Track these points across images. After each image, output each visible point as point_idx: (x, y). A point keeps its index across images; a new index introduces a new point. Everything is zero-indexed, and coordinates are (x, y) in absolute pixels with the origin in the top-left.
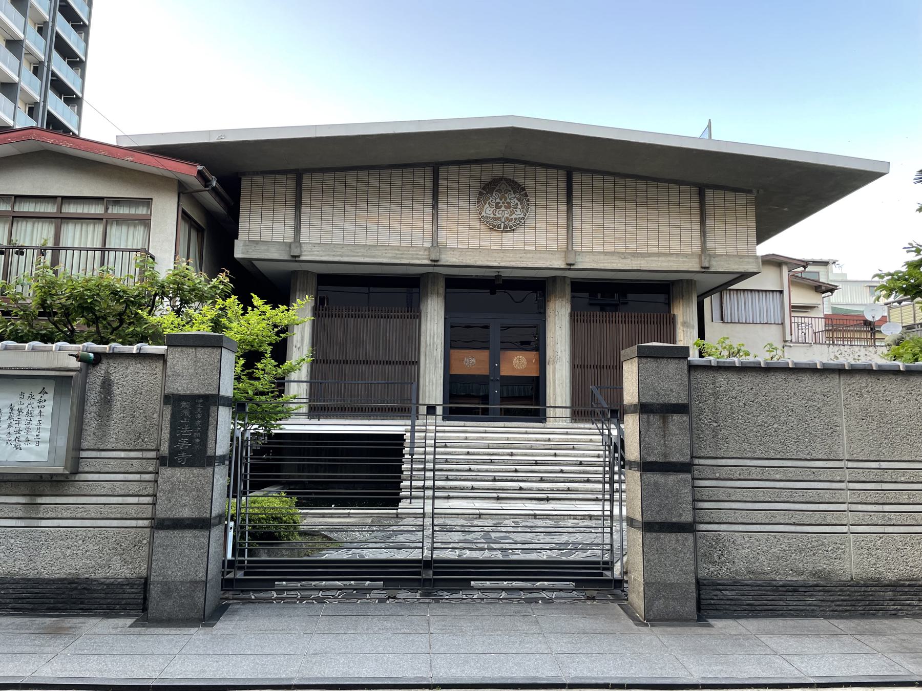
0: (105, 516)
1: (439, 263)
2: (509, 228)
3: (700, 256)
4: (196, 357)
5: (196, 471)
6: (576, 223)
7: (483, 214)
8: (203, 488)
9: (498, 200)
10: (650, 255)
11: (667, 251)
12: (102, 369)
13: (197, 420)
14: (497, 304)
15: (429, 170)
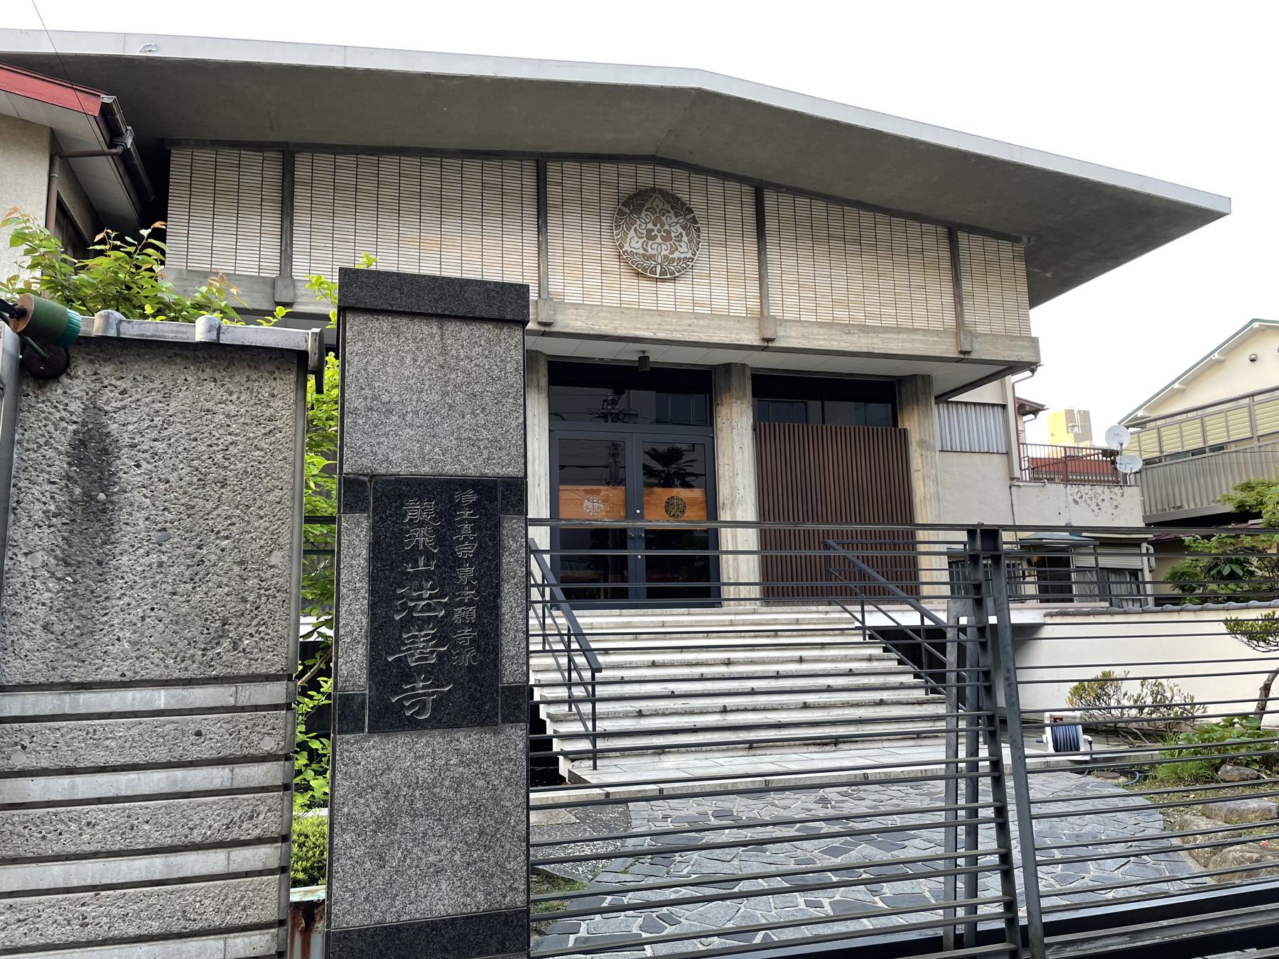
0: (102, 933)
1: (553, 329)
2: (668, 275)
3: (957, 335)
4: (444, 351)
5: (467, 740)
6: (773, 271)
7: (627, 247)
8: (496, 801)
9: (650, 226)
10: (886, 330)
11: (908, 324)
12: (74, 392)
13: (460, 562)
14: (634, 405)
15: (530, 167)
